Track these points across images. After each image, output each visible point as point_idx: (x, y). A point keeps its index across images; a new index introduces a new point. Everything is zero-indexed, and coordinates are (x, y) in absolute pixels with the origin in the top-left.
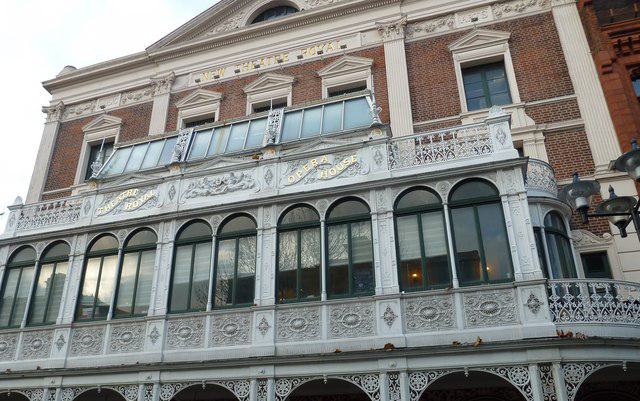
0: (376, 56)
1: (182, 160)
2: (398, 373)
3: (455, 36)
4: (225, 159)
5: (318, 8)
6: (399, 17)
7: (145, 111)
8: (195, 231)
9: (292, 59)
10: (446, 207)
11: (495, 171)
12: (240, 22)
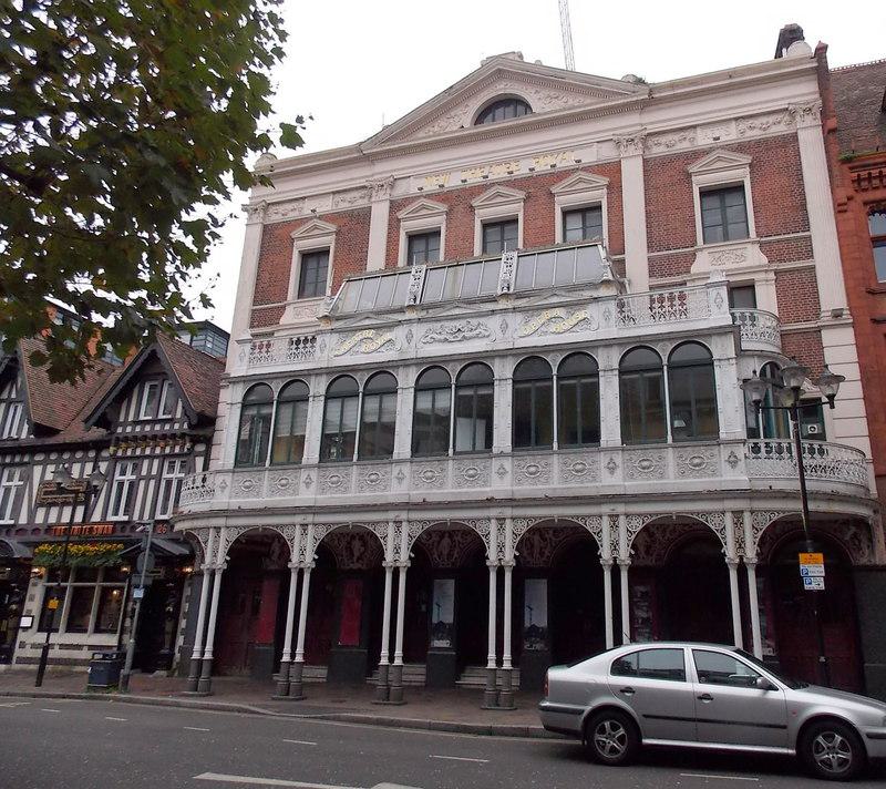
0: (612, 171)
1: (418, 302)
2: (617, 516)
3: (696, 155)
4: (462, 305)
5: (551, 112)
6: (639, 128)
7: (362, 218)
8: (434, 377)
9: (522, 170)
10: (665, 368)
11: (710, 335)
12: (465, 117)
